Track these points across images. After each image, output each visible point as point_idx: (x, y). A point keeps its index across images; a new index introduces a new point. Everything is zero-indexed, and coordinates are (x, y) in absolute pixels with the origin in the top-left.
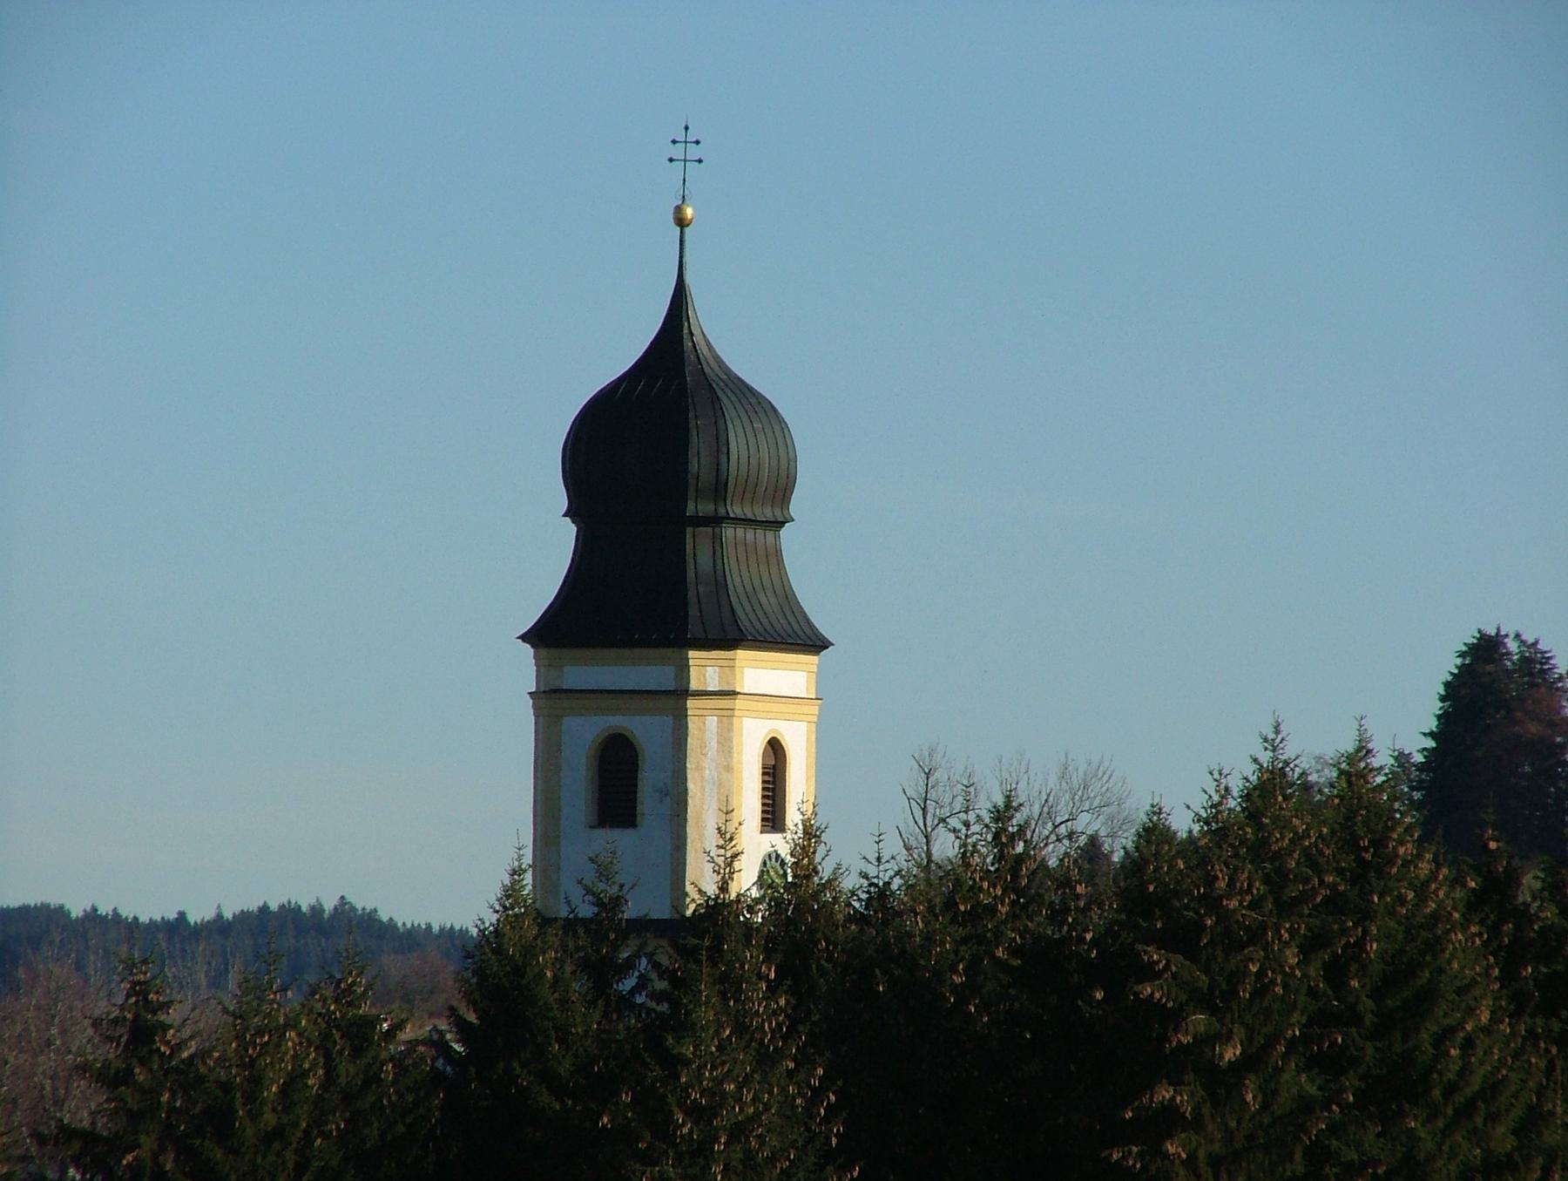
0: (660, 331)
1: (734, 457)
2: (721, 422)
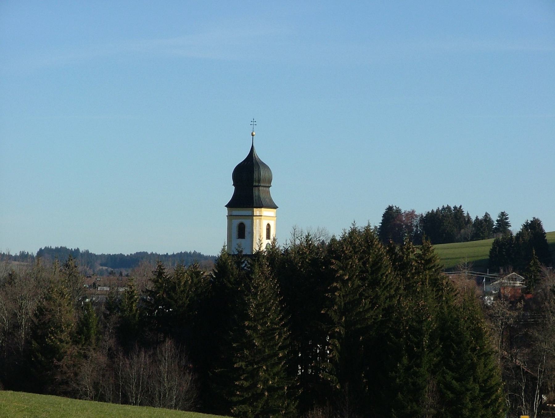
1: (261, 177)
2: (259, 170)
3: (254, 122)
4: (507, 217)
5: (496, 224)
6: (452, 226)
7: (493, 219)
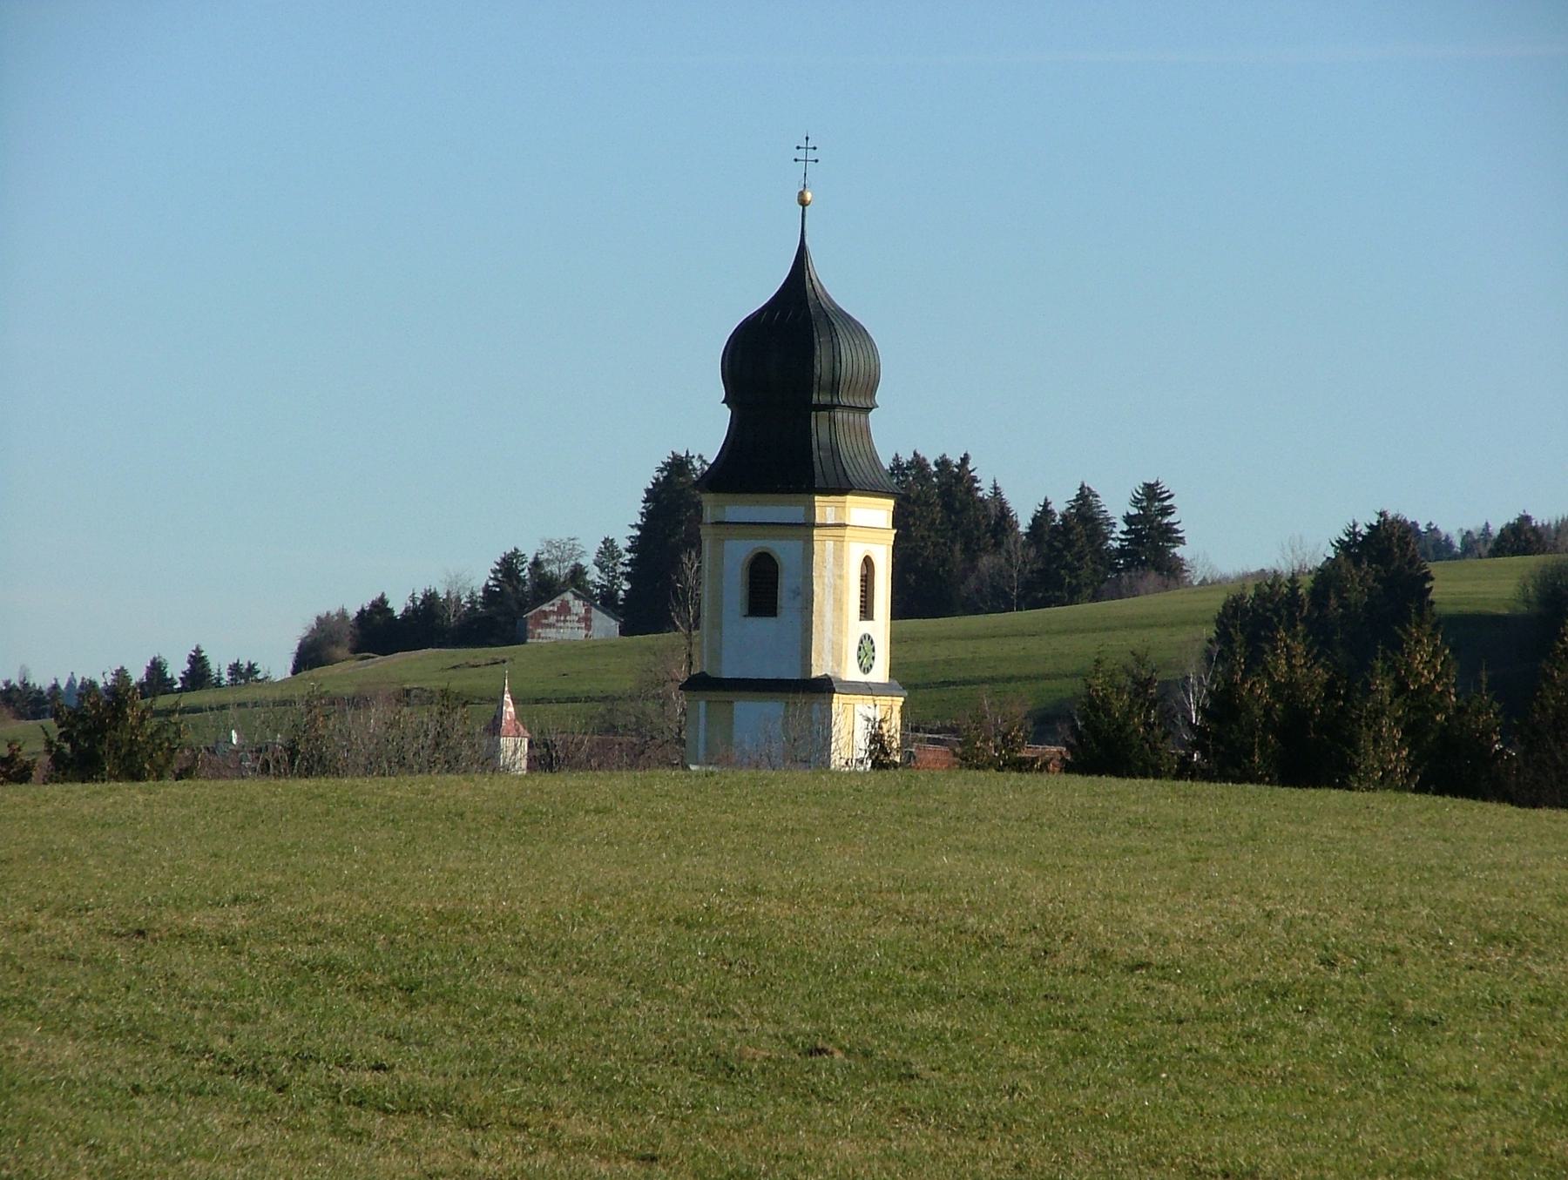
2: (835, 340)
3: (807, 148)
4: (1167, 503)
5: (1122, 532)
6: (942, 541)
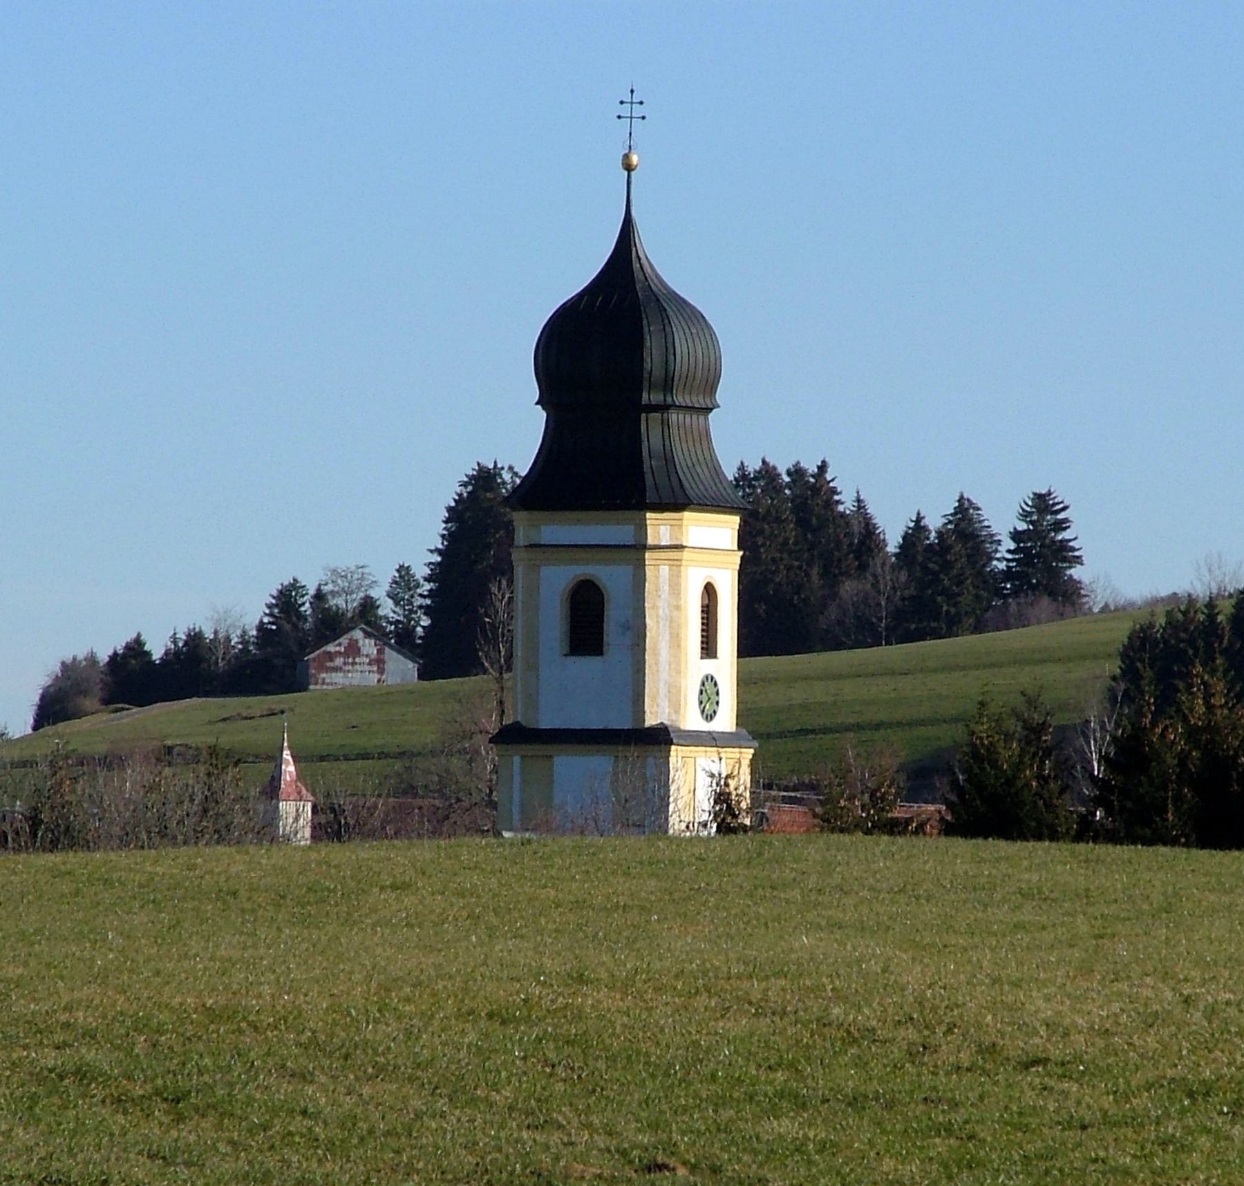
0: (611, 257)
1: (678, 360)
2: (668, 329)
3: (632, 103)
4: (1060, 516)
5: (1009, 551)
7: (994, 530)
